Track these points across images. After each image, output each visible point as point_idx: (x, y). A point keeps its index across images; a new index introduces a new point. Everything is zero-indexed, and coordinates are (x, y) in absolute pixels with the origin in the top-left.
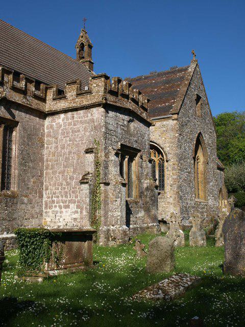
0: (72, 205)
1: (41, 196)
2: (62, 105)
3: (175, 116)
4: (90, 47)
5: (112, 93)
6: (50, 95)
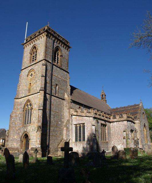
0: (120, 144)
1: (112, 142)
2: (115, 120)
3: (139, 120)
4: (105, 95)
5: (128, 117)
6: (112, 117)
